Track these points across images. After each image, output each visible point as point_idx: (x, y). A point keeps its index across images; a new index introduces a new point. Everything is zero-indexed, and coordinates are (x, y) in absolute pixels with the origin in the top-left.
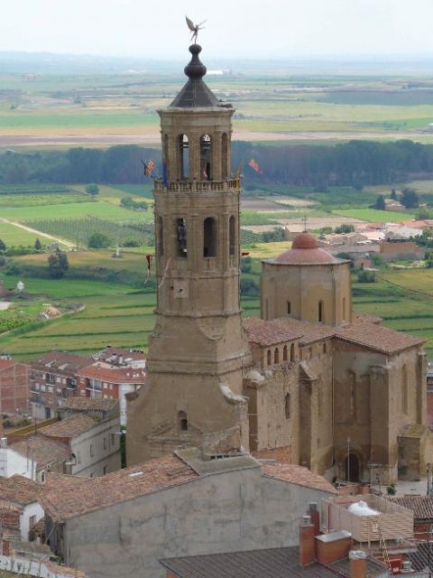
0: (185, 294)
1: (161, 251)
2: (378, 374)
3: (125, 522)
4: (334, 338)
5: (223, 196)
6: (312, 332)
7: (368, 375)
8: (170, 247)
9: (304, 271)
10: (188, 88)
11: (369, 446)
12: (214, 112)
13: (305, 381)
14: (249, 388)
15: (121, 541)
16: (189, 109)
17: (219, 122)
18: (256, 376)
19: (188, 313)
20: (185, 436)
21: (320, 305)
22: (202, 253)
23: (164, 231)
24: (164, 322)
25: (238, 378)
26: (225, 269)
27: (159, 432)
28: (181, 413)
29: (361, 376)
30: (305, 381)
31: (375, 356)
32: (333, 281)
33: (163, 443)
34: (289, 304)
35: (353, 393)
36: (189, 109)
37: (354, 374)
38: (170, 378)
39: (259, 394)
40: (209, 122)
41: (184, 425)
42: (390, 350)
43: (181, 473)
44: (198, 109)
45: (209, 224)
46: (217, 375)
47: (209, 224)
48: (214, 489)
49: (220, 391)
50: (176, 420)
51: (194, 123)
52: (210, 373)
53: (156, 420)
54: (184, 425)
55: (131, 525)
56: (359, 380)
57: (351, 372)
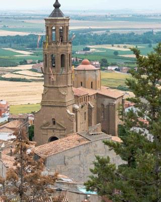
0: (55, 80)
1: (46, 65)
2: (112, 105)
3: (66, 158)
4: (97, 94)
5: (67, 47)
6: (91, 92)
7: (108, 106)
8: (49, 64)
9: (87, 73)
10: (55, 11)
11: (109, 129)
12: (64, 19)
13: (90, 108)
14: (74, 110)
15: (65, 164)
16: (56, 18)
17: (66, 22)
18: (77, 107)
19: (56, 86)
20: (54, 127)
21: (92, 83)
22: (60, 66)
23: (47, 59)
24: (47, 89)
25: (71, 107)
26: (68, 71)
27: (44, 126)
28: (53, 119)
29: (107, 106)
30: (90, 108)
31: (111, 99)
32: (96, 75)
33: (47, 129)
34: (81, 83)
35: (103, 112)
36: (56, 18)
37: (104, 105)
38: (50, 108)
39: (78, 113)
40: (62, 22)
41: (54, 123)
42: (116, 97)
43: (83, 140)
44: (59, 18)
45: (62, 56)
46: (66, 107)
47: (62, 56)
48: (96, 145)
49: (67, 111)
50: (51, 122)
51: (58, 23)
52: (63, 106)
53: (45, 122)
54: (54, 123)
55: (68, 158)
56: (105, 107)
57: (103, 105)
